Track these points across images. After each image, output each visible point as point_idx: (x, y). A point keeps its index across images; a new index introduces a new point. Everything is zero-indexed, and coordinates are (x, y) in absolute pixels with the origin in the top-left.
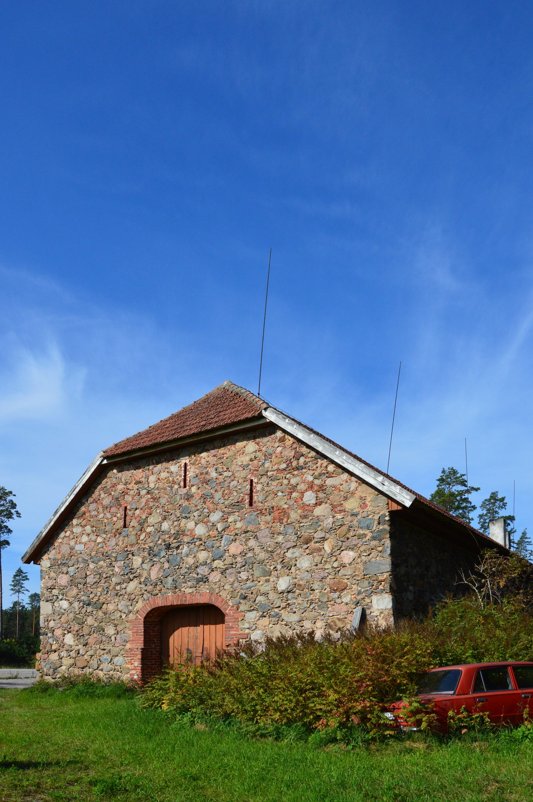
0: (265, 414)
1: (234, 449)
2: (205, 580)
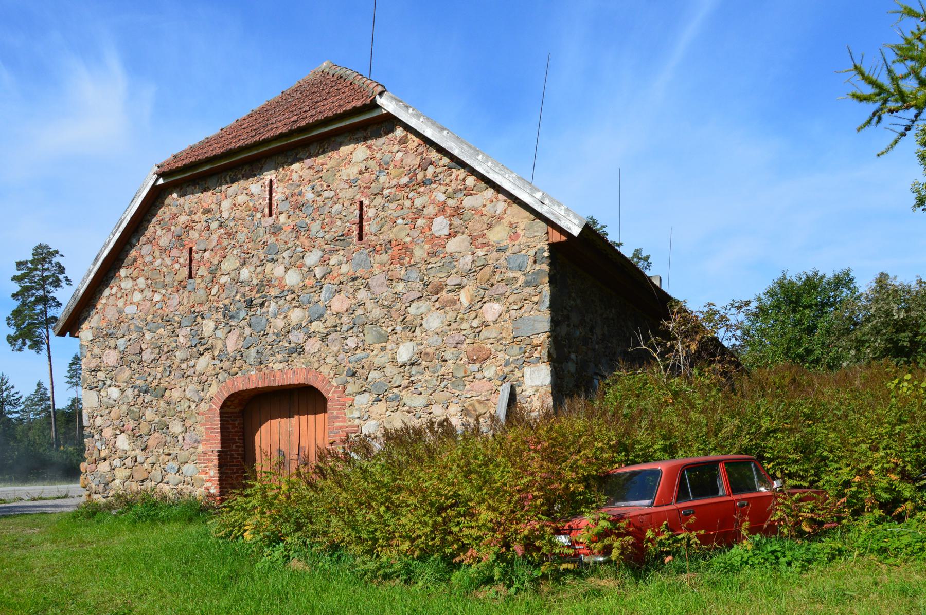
0: (380, 101)
1: (337, 157)
2: (299, 350)
